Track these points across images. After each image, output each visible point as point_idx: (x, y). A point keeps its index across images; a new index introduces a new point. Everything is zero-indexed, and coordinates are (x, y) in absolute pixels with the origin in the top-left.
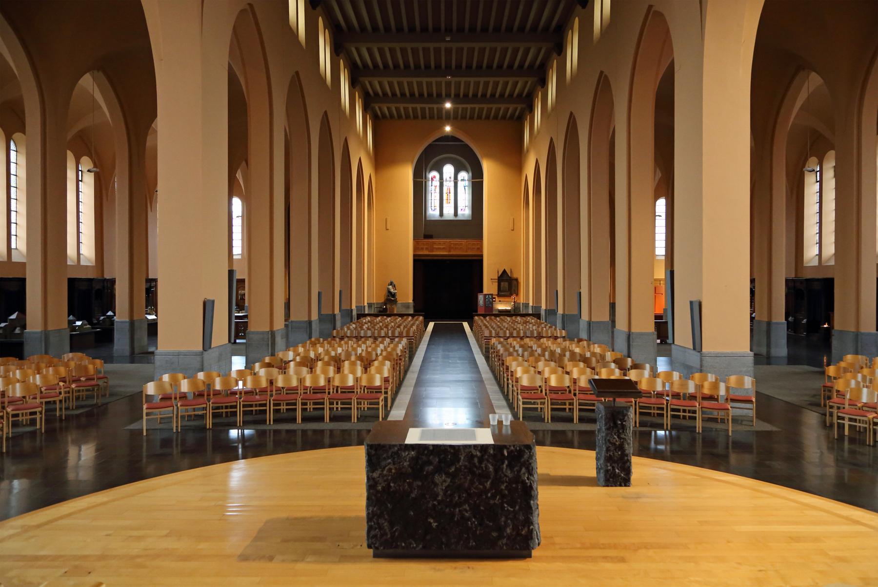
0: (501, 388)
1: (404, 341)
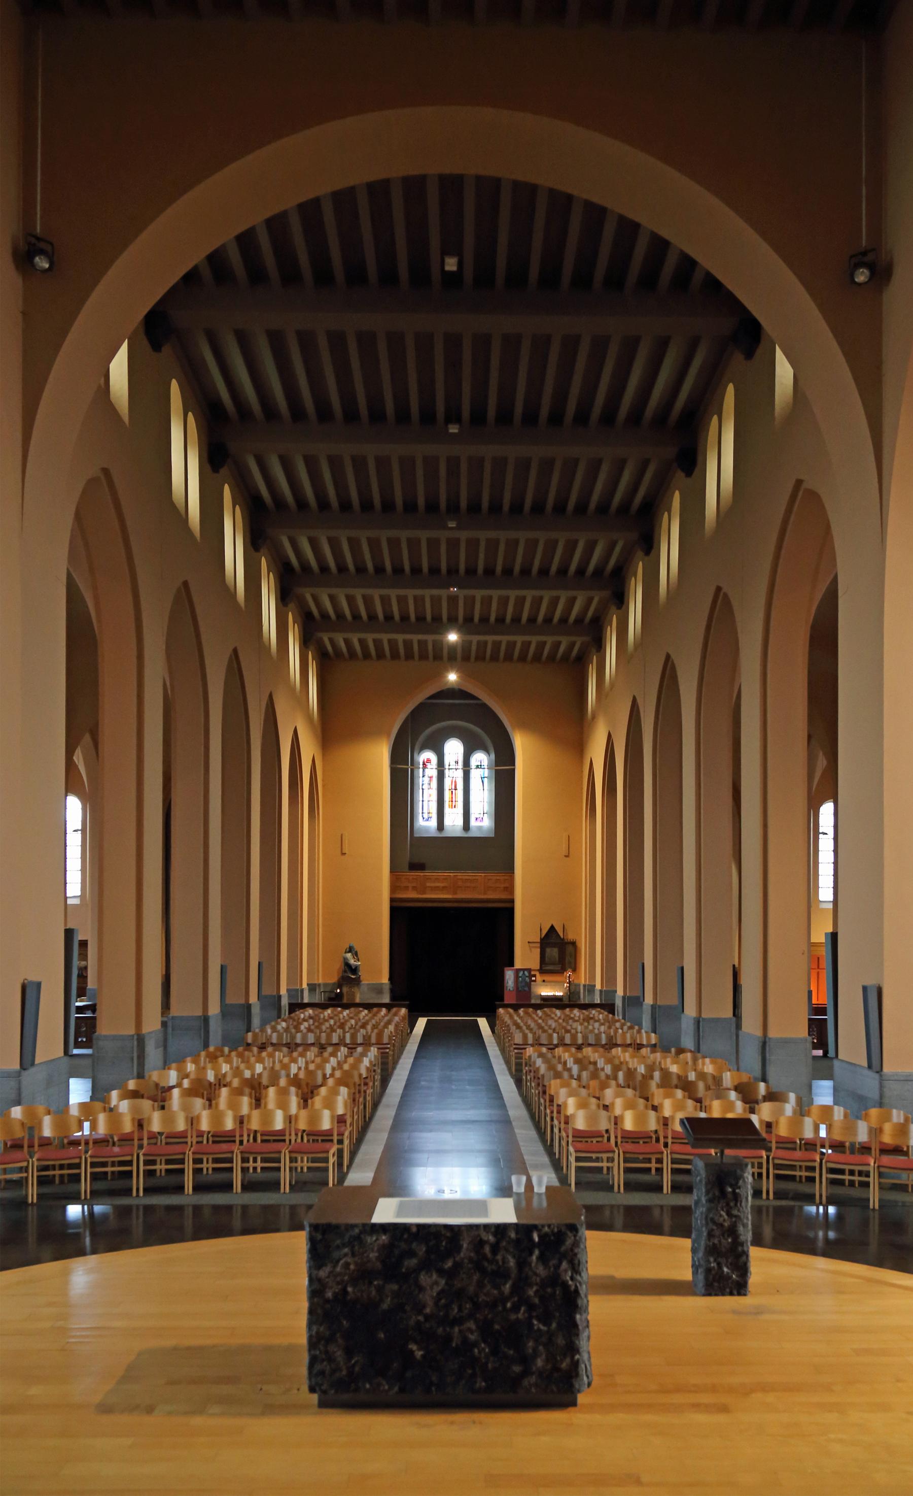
0: (542, 1134)
1: (373, 1052)
